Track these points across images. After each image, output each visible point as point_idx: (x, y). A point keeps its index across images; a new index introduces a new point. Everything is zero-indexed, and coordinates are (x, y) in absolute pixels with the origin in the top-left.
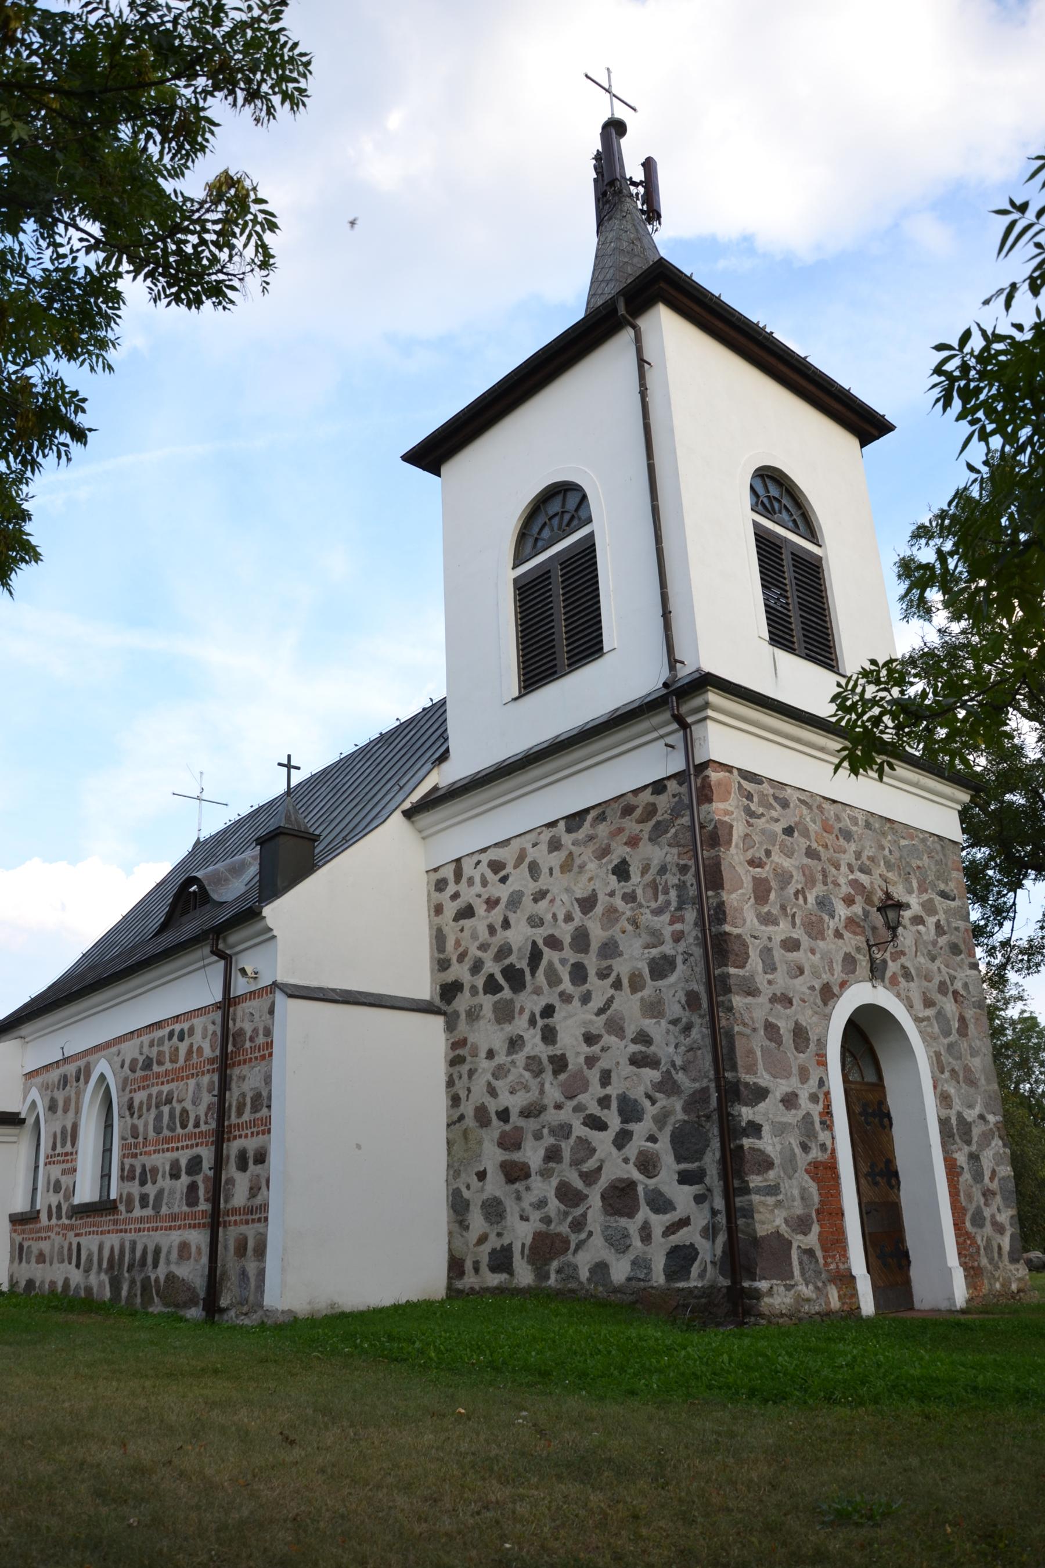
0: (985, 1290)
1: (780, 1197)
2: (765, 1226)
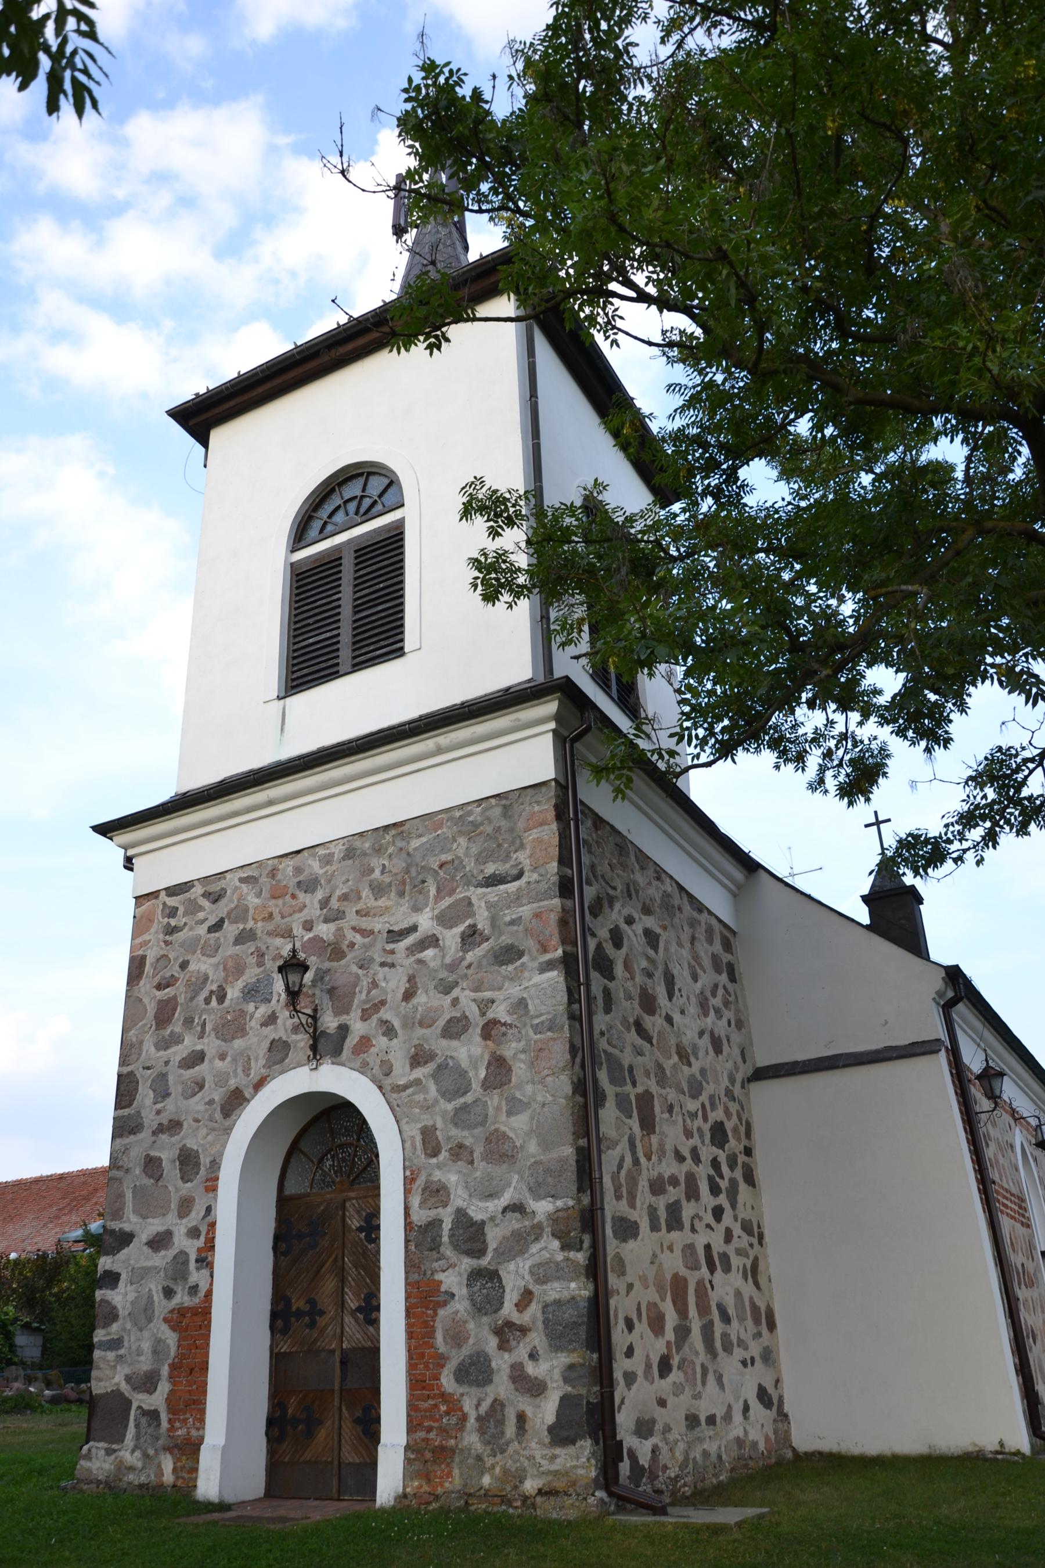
0: (455, 1480)
1: (122, 1352)
2: (102, 1384)
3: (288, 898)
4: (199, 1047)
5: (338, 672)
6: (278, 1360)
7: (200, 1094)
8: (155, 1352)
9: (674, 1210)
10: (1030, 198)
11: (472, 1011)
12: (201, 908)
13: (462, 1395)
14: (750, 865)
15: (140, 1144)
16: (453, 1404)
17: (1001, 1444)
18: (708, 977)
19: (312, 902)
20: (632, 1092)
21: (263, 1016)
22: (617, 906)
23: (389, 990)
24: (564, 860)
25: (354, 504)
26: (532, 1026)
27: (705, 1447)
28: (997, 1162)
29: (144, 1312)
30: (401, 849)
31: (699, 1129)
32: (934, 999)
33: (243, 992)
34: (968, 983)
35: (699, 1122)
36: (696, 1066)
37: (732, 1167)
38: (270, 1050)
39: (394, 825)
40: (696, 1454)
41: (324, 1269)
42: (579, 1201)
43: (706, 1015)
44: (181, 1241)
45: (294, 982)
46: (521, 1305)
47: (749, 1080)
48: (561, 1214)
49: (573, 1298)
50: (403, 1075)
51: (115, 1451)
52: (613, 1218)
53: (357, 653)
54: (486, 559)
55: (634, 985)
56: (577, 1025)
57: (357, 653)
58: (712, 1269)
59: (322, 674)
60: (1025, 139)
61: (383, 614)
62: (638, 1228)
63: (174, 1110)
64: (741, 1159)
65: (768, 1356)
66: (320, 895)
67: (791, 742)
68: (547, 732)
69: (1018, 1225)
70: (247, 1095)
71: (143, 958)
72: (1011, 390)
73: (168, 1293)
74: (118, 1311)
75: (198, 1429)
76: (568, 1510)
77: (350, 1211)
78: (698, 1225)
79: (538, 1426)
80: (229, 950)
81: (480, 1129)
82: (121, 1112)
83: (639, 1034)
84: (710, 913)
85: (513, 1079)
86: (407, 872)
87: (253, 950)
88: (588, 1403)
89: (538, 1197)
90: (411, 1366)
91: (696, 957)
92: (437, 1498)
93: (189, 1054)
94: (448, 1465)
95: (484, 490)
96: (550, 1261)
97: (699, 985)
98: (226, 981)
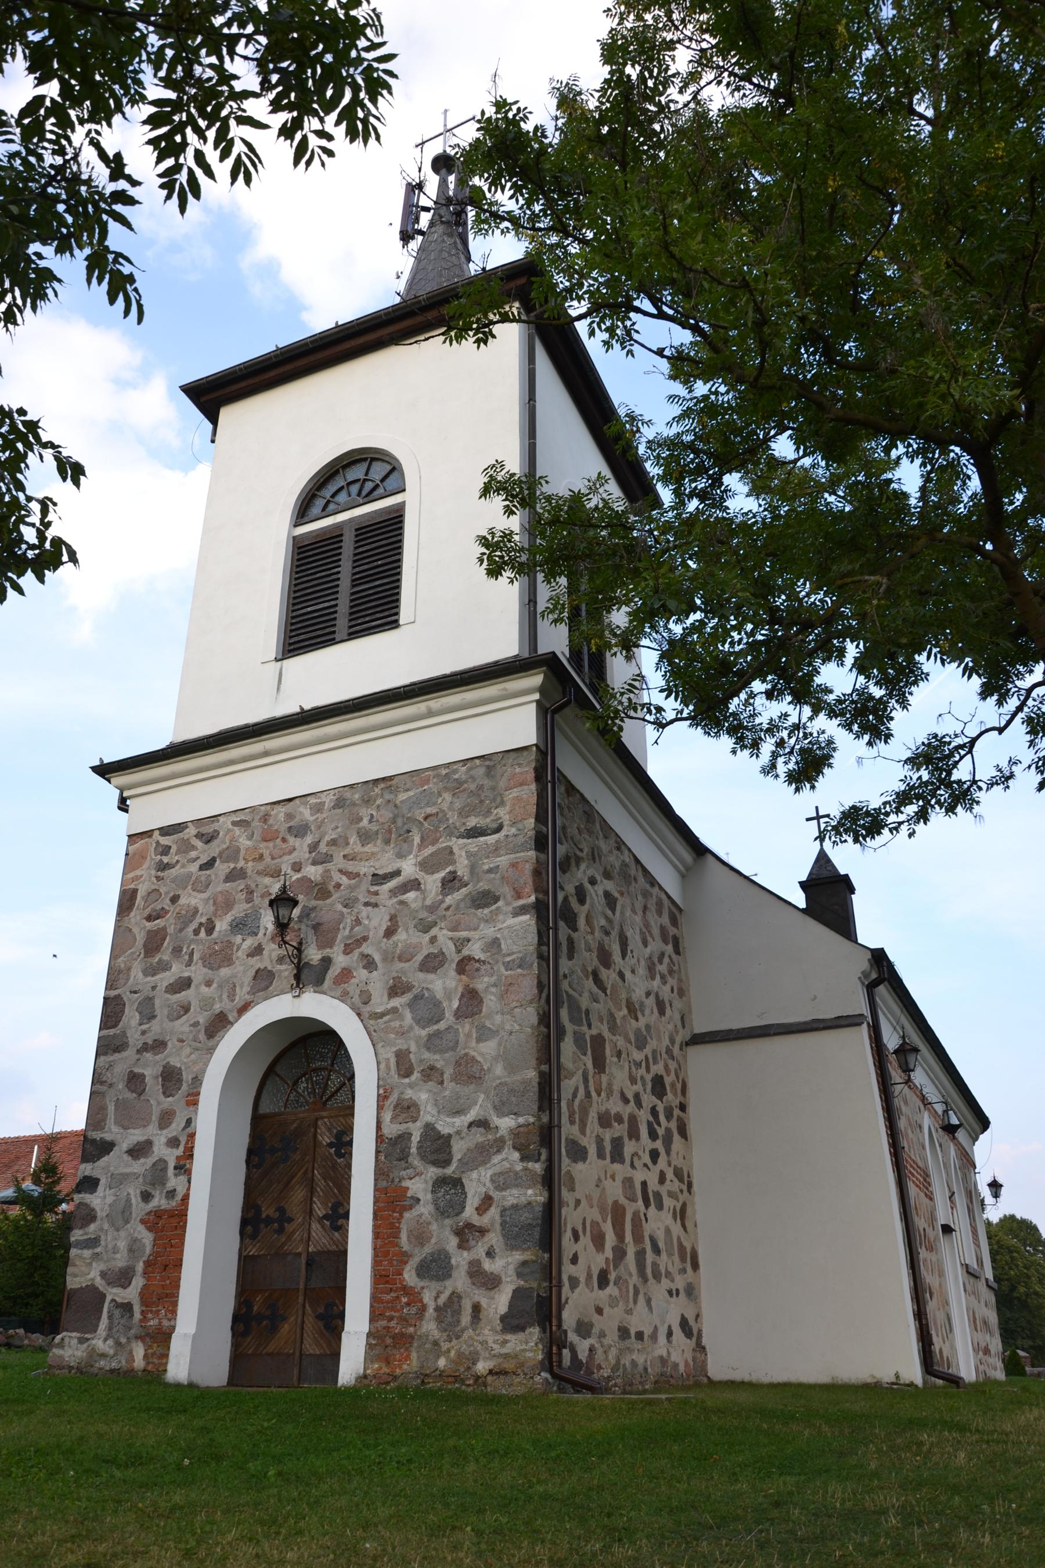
0: (412, 1363)
1: (98, 1250)
2: (77, 1279)
3: (278, 841)
4: (186, 974)
5: (334, 639)
6: (246, 1265)
7: (185, 1017)
8: (131, 1250)
9: (617, 1144)
10: (992, 259)
11: (449, 948)
12: (194, 848)
13: (423, 1288)
14: (700, 850)
15: (123, 1062)
16: (414, 1296)
17: (897, 1377)
18: (656, 946)
19: (301, 847)
20: (589, 1033)
21: (250, 947)
22: (583, 866)
23: (371, 927)
24: (541, 817)
25: (357, 486)
26: (503, 963)
27: (634, 1357)
28: (907, 1135)
29: (122, 1214)
30: (389, 801)
31: (642, 1078)
32: (860, 978)
33: (231, 925)
34: (891, 966)
35: (642, 1071)
36: (642, 1022)
37: (669, 1116)
38: (255, 978)
39: (384, 779)
40: (626, 1361)
41: (295, 1180)
42: (539, 1118)
43: (653, 978)
44: (161, 1150)
45: (283, 916)
46: (482, 1209)
47: (687, 1044)
48: (522, 1129)
49: (529, 1203)
50: (381, 1004)
51: (88, 1339)
52: (566, 1139)
53: (353, 623)
54: (493, 538)
55: (594, 939)
56: (545, 965)
57: (353, 623)
58: (647, 1204)
59: (319, 640)
60: (991, 210)
61: (380, 589)
62: (587, 1153)
63: (159, 1031)
64: (677, 1112)
65: (691, 1291)
66: (309, 839)
67: (748, 730)
68: (531, 702)
69: (922, 1195)
70: (231, 1019)
71: (135, 891)
72: (964, 416)
73: (146, 1197)
74: (96, 1212)
75: (170, 1320)
76: (517, 1386)
77: (322, 1129)
78: (636, 1163)
79: (491, 1315)
80: (219, 886)
81: (451, 1053)
82: (105, 1032)
83: (595, 983)
84: (661, 888)
85: (484, 1010)
86: (394, 822)
87: (242, 887)
88: (538, 1295)
89: (501, 1114)
90: (376, 1263)
91: (647, 925)
92: (395, 1378)
93: (176, 980)
94: (407, 1349)
95: (503, 473)
96: (510, 1170)
97: (648, 950)
98: (215, 915)
